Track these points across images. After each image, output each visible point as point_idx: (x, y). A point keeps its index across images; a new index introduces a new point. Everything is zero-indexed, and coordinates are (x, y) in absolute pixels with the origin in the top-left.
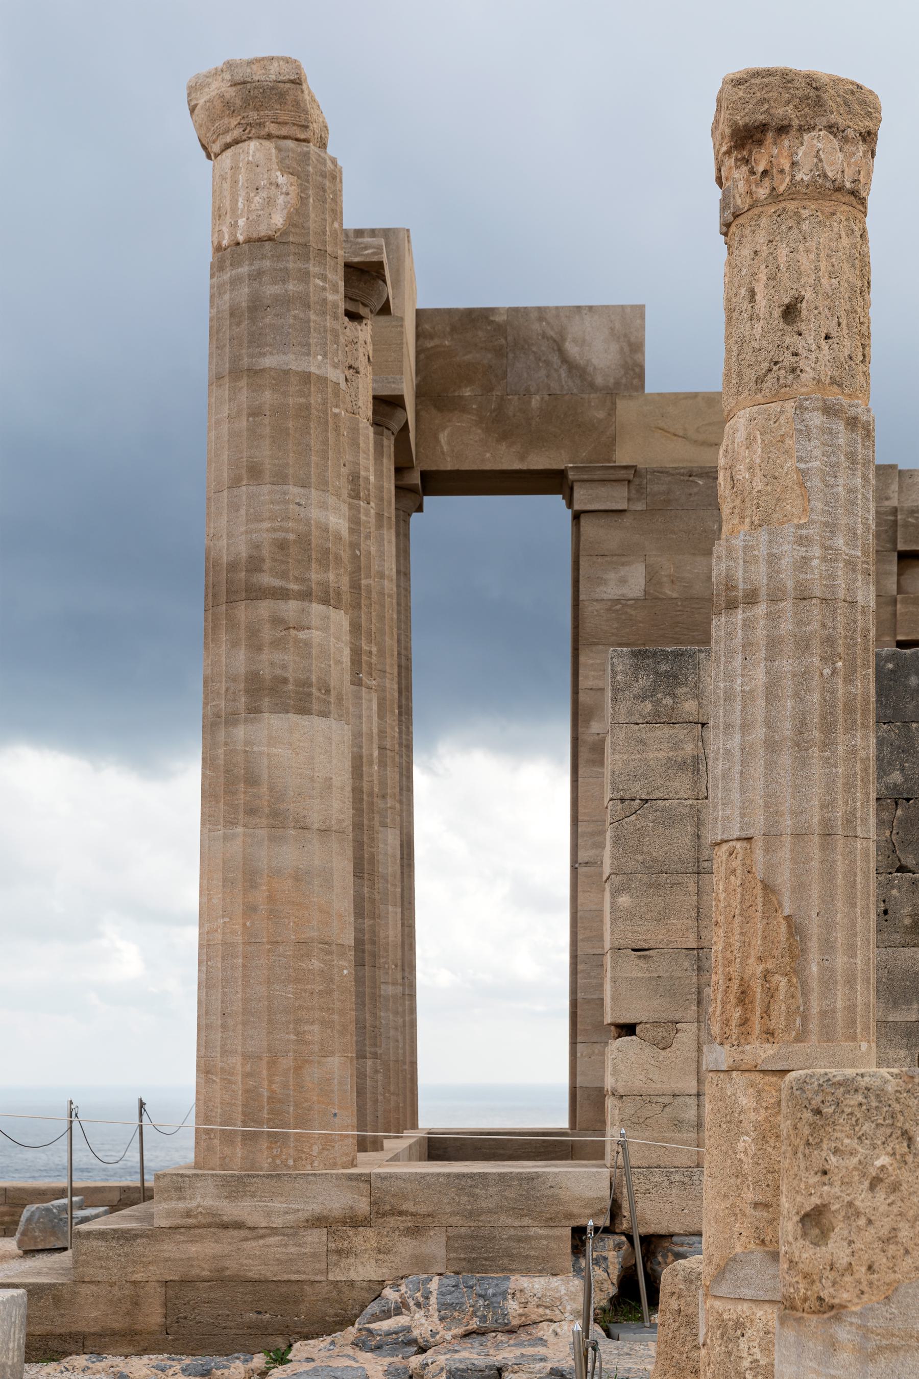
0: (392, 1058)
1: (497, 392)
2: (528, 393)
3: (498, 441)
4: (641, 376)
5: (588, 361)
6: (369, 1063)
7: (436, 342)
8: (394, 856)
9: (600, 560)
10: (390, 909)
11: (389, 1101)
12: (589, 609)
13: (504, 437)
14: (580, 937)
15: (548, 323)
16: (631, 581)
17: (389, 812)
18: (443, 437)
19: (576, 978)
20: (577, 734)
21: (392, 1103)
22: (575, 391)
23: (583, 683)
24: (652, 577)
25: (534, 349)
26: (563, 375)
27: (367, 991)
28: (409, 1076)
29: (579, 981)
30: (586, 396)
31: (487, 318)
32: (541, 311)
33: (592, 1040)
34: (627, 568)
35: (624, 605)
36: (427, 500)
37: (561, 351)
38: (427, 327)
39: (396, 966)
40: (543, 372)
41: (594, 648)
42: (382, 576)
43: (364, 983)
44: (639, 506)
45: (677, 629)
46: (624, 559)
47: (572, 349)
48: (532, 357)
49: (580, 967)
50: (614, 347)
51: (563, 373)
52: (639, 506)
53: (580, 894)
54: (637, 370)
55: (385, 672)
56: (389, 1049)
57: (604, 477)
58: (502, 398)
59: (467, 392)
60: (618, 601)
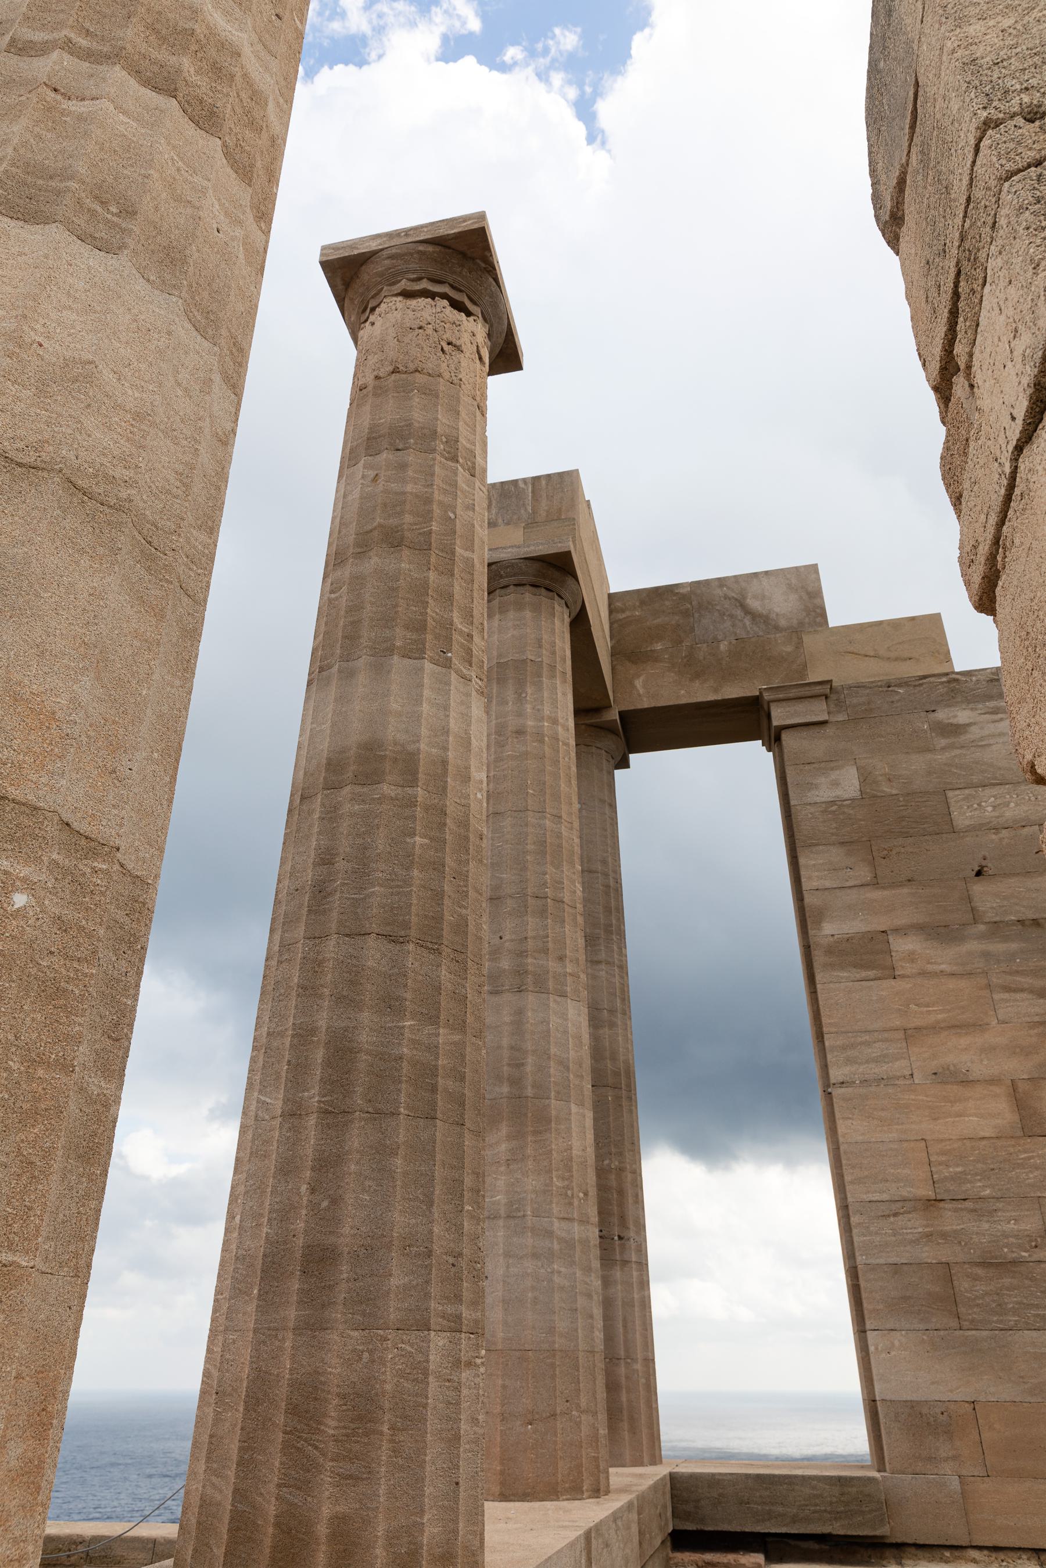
0: (582, 1346)
1: (687, 643)
2: (716, 641)
3: (691, 680)
4: (823, 615)
5: (769, 611)
6: (438, 1341)
7: (628, 613)
8: (579, 1037)
9: (807, 767)
10: (574, 1108)
11: (578, 1424)
12: (801, 815)
13: (697, 676)
14: (848, 1178)
15: (728, 588)
16: (846, 783)
17: (569, 979)
18: (639, 683)
19: (851, 1237)
20: (808, 942)
21: (585, 1430)
22: (761, 633)
23: (806, 885)
24: (865, 777)
25: (718, 608)
26: (748, 623)
27: (439, 1172)
28: (643, 1381)
29: (856, 1239)
30: (772, 636)
31: (672, 591)
32: (721, 582)
33: (888, 1326)
34: (838, 772)
35: (840, 806)
36: (633, 758)
37: (743, 606)
38: (619, 604)
39: (586, 1194)
40: (728, 624)
41: (814, 849)
42: (555, 721)
43: (433, 1157)
44: (841, 717)
45: (904, 823)
46: (832, 764)
47: (754, 604)
48: (716, 614)
49: (854, 1220)
50: (793, 597)
51: (747, 622)
52: (841, 717)
53: (840, 1123)
54: (818, 611)
55: (560, 817)
56: (576, 1330)
57: (799, 694)
58: (691, 647)
59: (659, 646)
60: (833, 803)
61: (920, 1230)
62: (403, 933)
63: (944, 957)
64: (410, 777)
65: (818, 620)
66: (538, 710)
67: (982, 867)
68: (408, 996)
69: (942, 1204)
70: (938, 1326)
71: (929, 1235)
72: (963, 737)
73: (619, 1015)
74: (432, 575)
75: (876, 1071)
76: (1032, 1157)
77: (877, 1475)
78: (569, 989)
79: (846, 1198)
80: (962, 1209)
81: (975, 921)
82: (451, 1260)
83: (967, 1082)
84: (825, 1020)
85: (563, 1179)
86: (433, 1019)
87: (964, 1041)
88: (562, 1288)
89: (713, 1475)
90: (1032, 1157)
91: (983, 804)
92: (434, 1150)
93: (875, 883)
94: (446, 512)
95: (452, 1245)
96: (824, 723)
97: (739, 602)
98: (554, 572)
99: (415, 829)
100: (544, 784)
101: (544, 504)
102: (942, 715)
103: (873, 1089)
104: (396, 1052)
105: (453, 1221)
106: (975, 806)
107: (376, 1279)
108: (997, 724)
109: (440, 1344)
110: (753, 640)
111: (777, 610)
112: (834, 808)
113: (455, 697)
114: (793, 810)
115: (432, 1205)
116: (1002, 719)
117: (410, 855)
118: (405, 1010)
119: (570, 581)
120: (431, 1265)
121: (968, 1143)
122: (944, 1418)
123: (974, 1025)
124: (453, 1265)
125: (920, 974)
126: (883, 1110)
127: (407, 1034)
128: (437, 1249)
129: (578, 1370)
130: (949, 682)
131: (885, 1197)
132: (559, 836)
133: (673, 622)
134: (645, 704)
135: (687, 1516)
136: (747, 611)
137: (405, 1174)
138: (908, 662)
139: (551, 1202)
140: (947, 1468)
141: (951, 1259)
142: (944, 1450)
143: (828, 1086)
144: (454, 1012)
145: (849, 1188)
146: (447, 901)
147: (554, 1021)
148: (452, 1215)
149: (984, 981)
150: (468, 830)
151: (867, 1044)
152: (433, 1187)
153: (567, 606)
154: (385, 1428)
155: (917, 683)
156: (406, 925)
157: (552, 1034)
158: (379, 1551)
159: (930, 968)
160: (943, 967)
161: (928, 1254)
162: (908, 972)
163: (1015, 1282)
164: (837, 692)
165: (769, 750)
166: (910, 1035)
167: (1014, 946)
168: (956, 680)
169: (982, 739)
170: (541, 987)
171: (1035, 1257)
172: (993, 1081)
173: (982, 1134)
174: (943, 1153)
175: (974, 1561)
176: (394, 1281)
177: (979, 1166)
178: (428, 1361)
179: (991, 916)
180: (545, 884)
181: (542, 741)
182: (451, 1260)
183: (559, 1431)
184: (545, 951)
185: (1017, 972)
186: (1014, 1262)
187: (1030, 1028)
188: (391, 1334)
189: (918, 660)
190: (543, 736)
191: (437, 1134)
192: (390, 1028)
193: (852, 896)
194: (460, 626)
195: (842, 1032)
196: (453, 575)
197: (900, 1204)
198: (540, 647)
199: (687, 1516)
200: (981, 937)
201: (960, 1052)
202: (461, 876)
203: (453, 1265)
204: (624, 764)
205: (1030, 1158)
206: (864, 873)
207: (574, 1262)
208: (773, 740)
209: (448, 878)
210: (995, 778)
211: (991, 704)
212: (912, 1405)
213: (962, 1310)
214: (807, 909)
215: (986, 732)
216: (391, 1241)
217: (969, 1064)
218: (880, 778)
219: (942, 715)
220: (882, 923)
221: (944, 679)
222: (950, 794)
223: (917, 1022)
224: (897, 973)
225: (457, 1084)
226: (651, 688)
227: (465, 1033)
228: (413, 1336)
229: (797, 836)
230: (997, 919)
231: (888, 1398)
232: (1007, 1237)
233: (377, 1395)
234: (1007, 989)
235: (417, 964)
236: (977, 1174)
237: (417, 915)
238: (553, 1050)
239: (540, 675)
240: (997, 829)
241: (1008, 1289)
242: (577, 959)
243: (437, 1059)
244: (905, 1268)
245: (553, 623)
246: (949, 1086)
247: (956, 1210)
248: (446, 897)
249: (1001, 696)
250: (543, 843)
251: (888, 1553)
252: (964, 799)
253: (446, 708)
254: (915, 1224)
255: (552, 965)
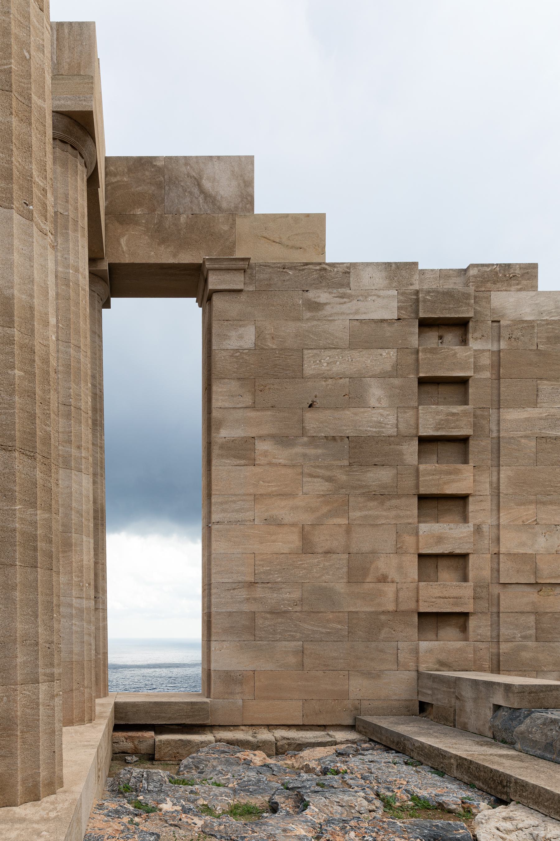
0: (86, 658)
1: (158, 212)
2: (178, 213)
3: (159, 244)
6: (43, 687)
7: (118, 178)
9: (226, 323)
12: (219, 356)
13: (163, 241)
14: (213, 571)
15: (191, 167)
17: (83, 460)
21: (86, 695)
22: (209, 212)
23: (215, 404)
24: (259, 335)
25: (182, 184)
27: (40, 598)
28: (102, 662)
30: (216, 215)
31: (151, 163)
32: (187, 160)
33: (222, 640)
34: (243, 329)
37: (199, 185)
38: (112, 168)
39: (89, 584)
40: (188, 199)
41: (222, 381)
42: (77, 270)
44: (251, 288)
45: (276, 369)
46: (241, 323)
47: (207, 185)
49: (213, 591)
50: (234, 183)
52: (251, 288)
54: (249, 198)
55: (79, 347)
56: (83, 652)
59: (139, 212)
61: (244, 596)
62: (10, 444)
63: (282, 455)
64: (7, 319)
65: (248, 206)
66: (66, 259)
67: (313, 402)
68: (17, 488)
69: (257, 585)
70: (245, 639)
71: (248, 599)
72: (320, 313)
73: (99, 477)
74: (15, 121)
75: (236, 516)
76: (304, 564)
77: (208, 700)
78: (83, 467)
79: (210, 580)
80: (266, 587)
81: (303, 435)
82: (48, 645)
83: (280, 525)
84: (214, 487)
85: (78, 577)
86: (33, 505)
87: (283, 503)
88: (77, 632)
89: (135, 702)
90: (304, 564)
91: (322, 361)
92: (37, 586)
93: (253, 407)
94: (22, 49)
95: (48, 637)
96: (240, 291)
97: (198, 182)
98: (77, 128)
99: (14, 363)
100: (70, 320)
101: (66, 54)
102: (311, 295)
103: (233, 526)
104: (11, 526)
105: (48, 625)
106: (318, 361)
107: (8, 659)
108: (341, 306)
109: (44, 689)
110: (203, 216)
111: (222, 193)
112: (238, 354)
113: (36, 249)
114: (213, 353)
115: (37, 618)
116: (345, 303)
117: (12, 384)
118: (15, 499)
119: (89, 141)
120: (38, 650)
121: (275, 556)
122: (241, 677)
123: (290, 495)
124: (49, 648)
125: (268, 464)
126: (236, 537)
127: (18, 515)
128: (41, 641)
129: (84, 670)
130: (320, 270)
131: (230, 581)
132: (79, 362)
133: (150, 192)
134: (127, 259)
135: (121, 719)
136: (202, 191)
137: (21, 600)
138: (299, 250)
139: (72, 589)
140: (238, 696)
141: (257, 610)
142: (238, 689)
143: (210, 523)
144: (44, 499)
145: (213, 576)
146: (38, 421)
147: (74, 486)
148: (47, 621)
149: (300, 470)
150: (48, 367)
151: (234, 502)
152: (38, 607)
153: (86, 166)
154: (19, 733)
155: (301, 268)
156: (12, 438)
157: (73, 495)
158: (19, 788)
159: (274, 461)
160: (281, 461)
161: (246, 608)
162: (262, 462)
163: (283, 620)
164: (252, 268)
165: (200, 306)
166: (257, 498)
167: (320, 451)
168: (325, 269)
169: (331, 315)
170: (67, 465)
171: (294, 610)
172: (293, 525)
173: (283, 551)
174: (262, 560)
175: (242, 730)
176: (19, 660)
177: (278, 567)
178: (39, 699)
179: (312, 433)
180: (70, 395)
181: (68, 285)
182: (48, 645)
183: (74, 697)
184: (70, 442)
185: (318, 466)
186: (285, 612)
187: (318, 498)
188: (19, 687)
189: (305, 250)
190: (69, 280)
191: (39, 576)
192: (6, 510)
193: (239, 414)
194: (37, 180)
195: (222, 495)
196: (30, 124)
197: (237, 584)
198: (67, 202)
199: (121, 719)
200: (304, 445)
201: (281, 509)
202: (46, 402)
203: (49, 648)
204: (107, 305)
205: (302, 564)
206: (248, 400)
207: (83, 619)
208: (206, 300)
209: (38, 403)
210: (332, 344)
211: (341, 290)
212: (227, 672)
213: (257, 632)
214: (213, 420)
215: (335, 311)
216: (16, 639)
217: (283, 515)
218: (268, 336)
219: (311, 295)
220: (252, 432)
221: (318, 268)
222: (305, 352)
223: (261, 491)
224: (256, 463)
225: (48, 545)
226: (132, 247)
227: (51, 513)
228: (30, 687)
229: (214, 371)
230: (315, 435)
231: (217, 669)
232: (284, 601)
233: (13, 717)
234: (311, 476)
235: (21, 466)
236: (276, 571)
237: (19, 431)
238: (74, 504)
239: (67, 229)
240: (326, 378)
241: (279, 624)
242: (88, 448)
243: (36, 530)
244: (234, 614)
245: (77, 181)
246: (272, 527)
247: (263, 588)
248: (37, 418)
249: (348, 285)
250: (68, 366)
251: (207, 729)
252: (312, 356)
253: (31, 259)
254: (243, 594)
255: (74, 451)
